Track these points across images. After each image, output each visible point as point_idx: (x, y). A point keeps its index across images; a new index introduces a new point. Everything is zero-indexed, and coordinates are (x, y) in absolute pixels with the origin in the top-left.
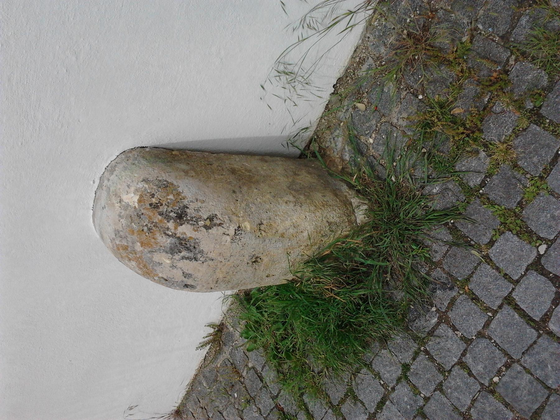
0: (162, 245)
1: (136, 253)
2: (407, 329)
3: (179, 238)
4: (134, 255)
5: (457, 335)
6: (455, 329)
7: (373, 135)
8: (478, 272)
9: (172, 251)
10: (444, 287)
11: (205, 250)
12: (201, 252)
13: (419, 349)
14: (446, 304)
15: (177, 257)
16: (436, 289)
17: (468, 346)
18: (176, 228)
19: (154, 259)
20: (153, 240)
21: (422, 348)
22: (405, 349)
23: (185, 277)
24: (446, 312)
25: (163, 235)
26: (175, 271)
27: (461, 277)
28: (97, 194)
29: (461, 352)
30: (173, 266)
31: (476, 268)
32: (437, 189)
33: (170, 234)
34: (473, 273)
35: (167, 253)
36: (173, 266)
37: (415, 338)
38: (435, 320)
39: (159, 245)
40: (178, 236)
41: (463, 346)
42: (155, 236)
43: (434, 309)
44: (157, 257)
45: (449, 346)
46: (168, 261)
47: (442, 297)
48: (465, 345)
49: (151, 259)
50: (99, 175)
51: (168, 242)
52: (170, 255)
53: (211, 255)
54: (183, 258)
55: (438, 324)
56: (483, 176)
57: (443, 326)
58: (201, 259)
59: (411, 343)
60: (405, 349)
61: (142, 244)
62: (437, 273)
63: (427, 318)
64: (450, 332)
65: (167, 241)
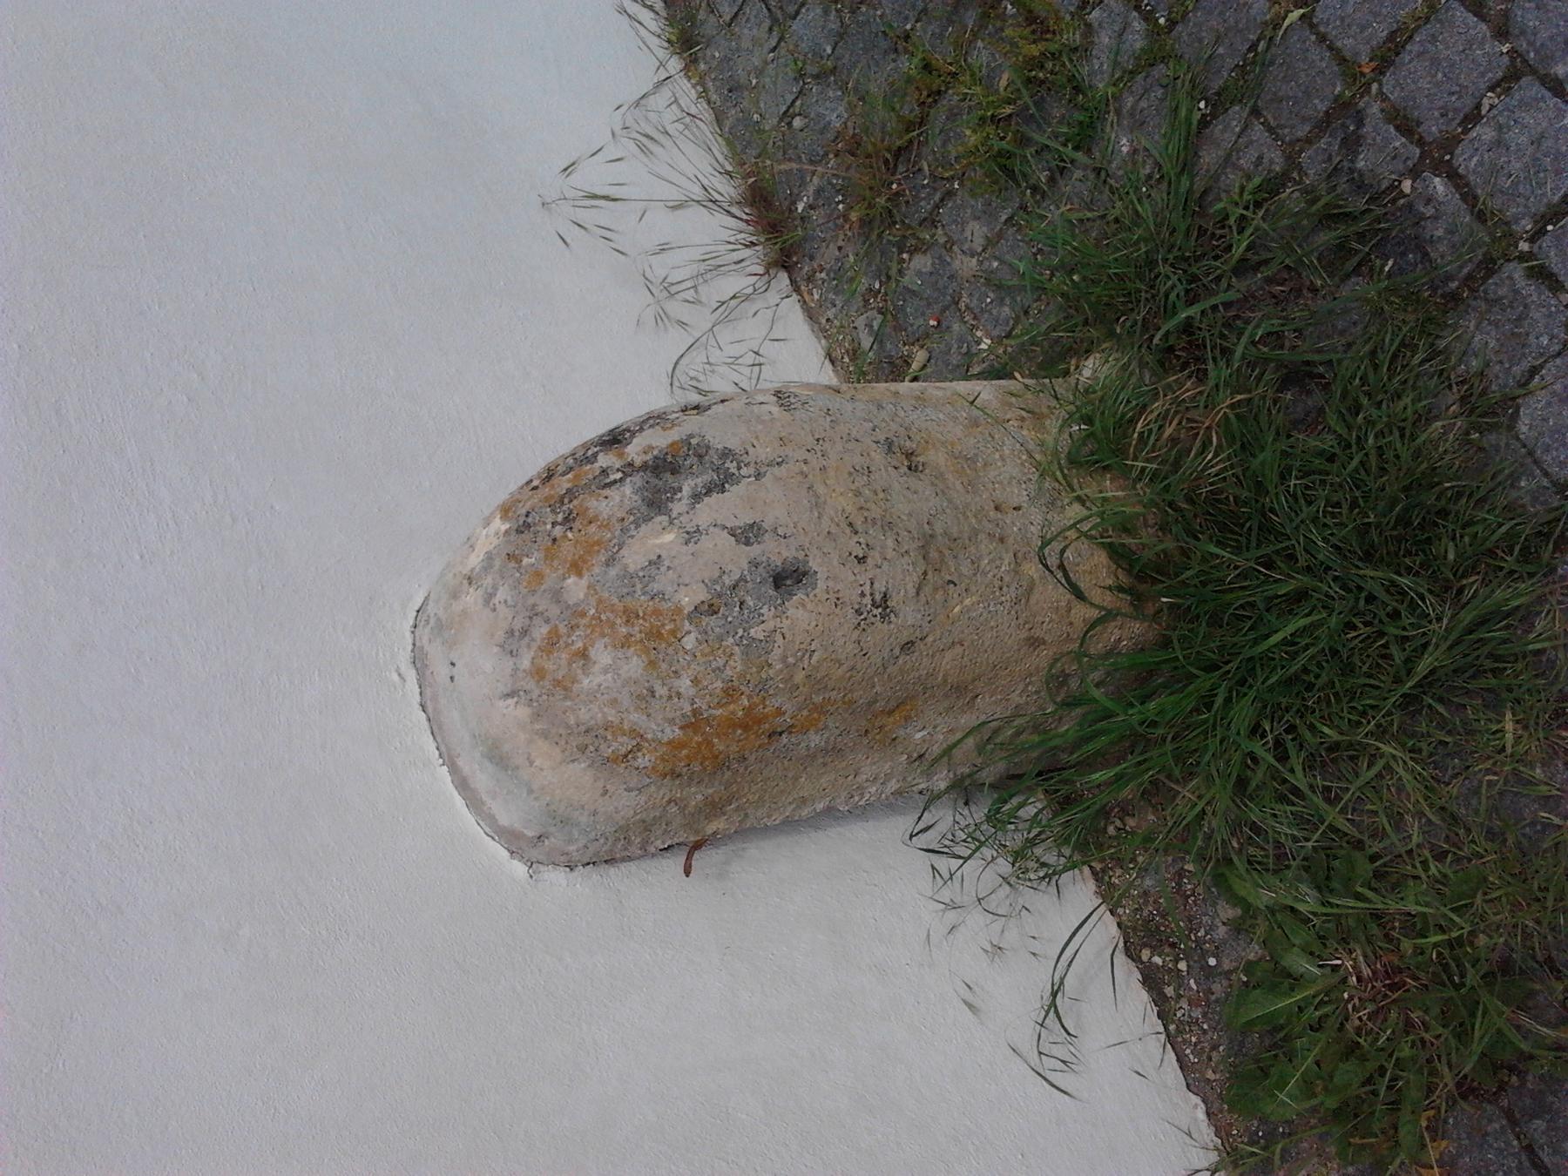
0: (620, 515)
1: (583, 614)
2: (1454, 298)
3: (644, 467)
4: (584, 621)
5: (1492, 107)
6: (1473, 117)
7: (979, 334)
8: (1331, 31)
9: (656, 503)
10: (1352, 144)
11: (733, 444)
12: (726, 454)
13: (1522, 257)
14: (1399, 142)
15: (677, 507)
16: (1351, 170)
17: (1534, 72)
18: (621, 455)
19: (631, 569)
20: (593, 528)
21: (1524, 246)
22: (1519, 319)
23: (747, 543)
24: (1421, 142)
25: (607, 492)
26: (706, 543)
27: (1334, 86)
28: (430, 710)
29: (1548, 94)
30: (692, 536)
31: (1322, 38)
32: (1124, 141)
33: (619, 475)
34: (1331, 48)
35: (648, 519)
36: (692, 536)
37: (1489, 266)
38: (1439, 185)
39: (614, 520)
40: (638, 462)
41: (1529, 88)
42: (591, 513)
43: (1407, 186)
44: (634, 557)
45: (1524, 139)
46: (669, 537)
47: (1382, 153)
48: (1525, 81)
49: (629, 577)
50: (404, 656)
51: (627, 494)
52: (659, 518)
53: (764, 452)
54: (696, 497)
55: (1453, 176)
56: (1135, 14)
57: (1467, 160)
58: (744, 471)
59: (1496, 287)
60: (1519, 319)
61: (577, 568)
62: (1313, 165)
63: (1429, 211)
64: (1484, 133)
65: (624, 496)
